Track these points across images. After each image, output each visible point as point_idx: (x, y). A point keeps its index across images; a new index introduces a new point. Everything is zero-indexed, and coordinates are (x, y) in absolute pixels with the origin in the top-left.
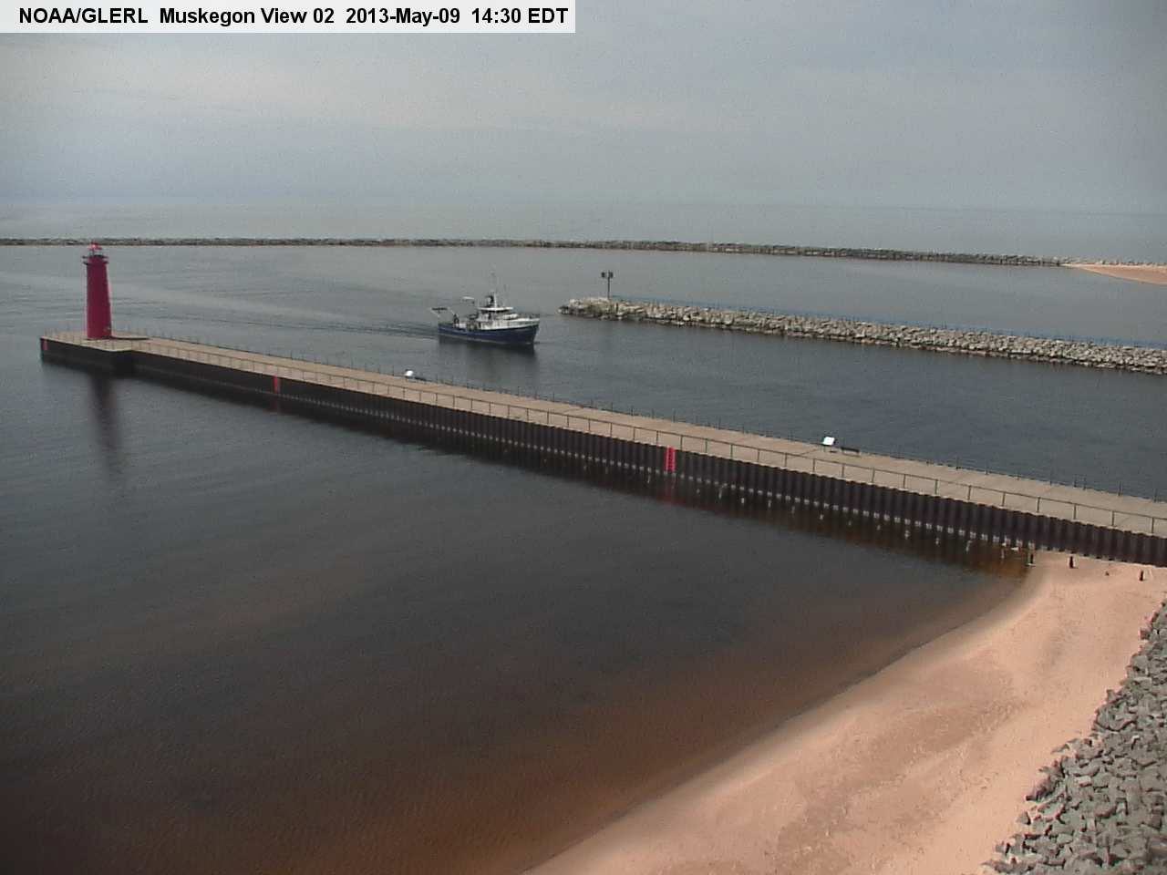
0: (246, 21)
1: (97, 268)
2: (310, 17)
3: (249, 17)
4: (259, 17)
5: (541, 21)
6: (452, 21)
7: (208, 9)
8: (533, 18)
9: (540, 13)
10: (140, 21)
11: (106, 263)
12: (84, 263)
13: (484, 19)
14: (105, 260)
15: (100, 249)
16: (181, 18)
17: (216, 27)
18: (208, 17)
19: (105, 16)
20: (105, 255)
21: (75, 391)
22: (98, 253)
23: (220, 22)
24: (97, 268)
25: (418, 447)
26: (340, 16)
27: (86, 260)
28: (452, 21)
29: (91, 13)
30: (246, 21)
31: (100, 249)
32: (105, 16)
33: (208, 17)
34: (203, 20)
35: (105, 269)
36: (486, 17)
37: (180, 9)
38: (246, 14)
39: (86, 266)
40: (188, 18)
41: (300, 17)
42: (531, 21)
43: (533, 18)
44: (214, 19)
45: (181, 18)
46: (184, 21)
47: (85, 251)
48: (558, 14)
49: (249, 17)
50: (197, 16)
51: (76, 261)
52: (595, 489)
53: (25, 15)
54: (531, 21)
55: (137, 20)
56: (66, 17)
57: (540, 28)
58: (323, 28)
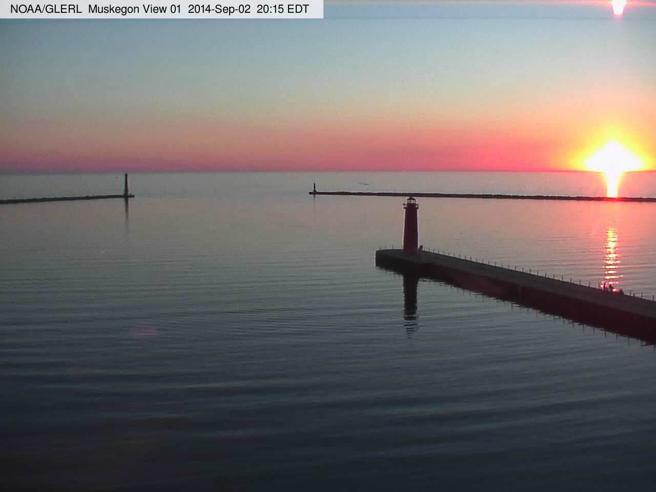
0: (135, 12)
1: (411, 212)
2: (168, 10)
3: (136, 9)
4: (142, 10)
5: (295, 11)
6: (108, 8)
7: (114, 5)
8: (290, 10)
9: (294, 7)
10: (77, 12)
11: (417, 208)
12: (405, 208)
13: (206, 10)
14: (416, 206)
15: (414, 199)
16: (100, 11)
17: (119, 16)
18: (114, 9)
19: (58, 9)
20: (417, 203)
21: (395, 282)
22: (412, 202)
23: (121, 12)
24: (411, 212)
25: (475, 293)
26: (185, 9)
27: (405, 206)
28: (108, 8)
29: (51, 7)
30: (135, 12)
31: (414, 199)
32: (58, 9)
33: (114, 9)
34: (111, 11)
35: (416, 211)
36: (208, 9)
37: (100, 6)
38: (135, 8)
39: (405, 210)
40: (104, 10)
41: (163, 10)
42: (289, 12)
43: (290, 10)
44: (226, 11)
45: (100, 11)
46: (102, 12)
47: (405, 200)
48: (304, 7)
49: (136, 9)
50: (109, 9)
51: (398, 207)
52: (576, 324)
53: (16, 9)
54: (289, 12)
55: (76, 11)
56: (36, 10)
57: (294, 16)
58: (244, 16)
